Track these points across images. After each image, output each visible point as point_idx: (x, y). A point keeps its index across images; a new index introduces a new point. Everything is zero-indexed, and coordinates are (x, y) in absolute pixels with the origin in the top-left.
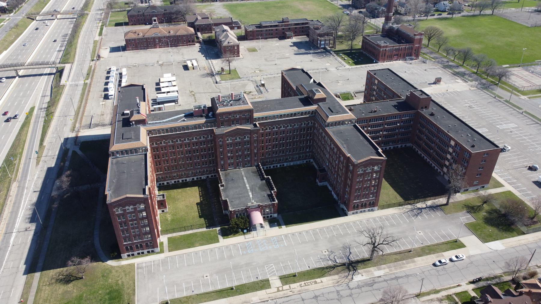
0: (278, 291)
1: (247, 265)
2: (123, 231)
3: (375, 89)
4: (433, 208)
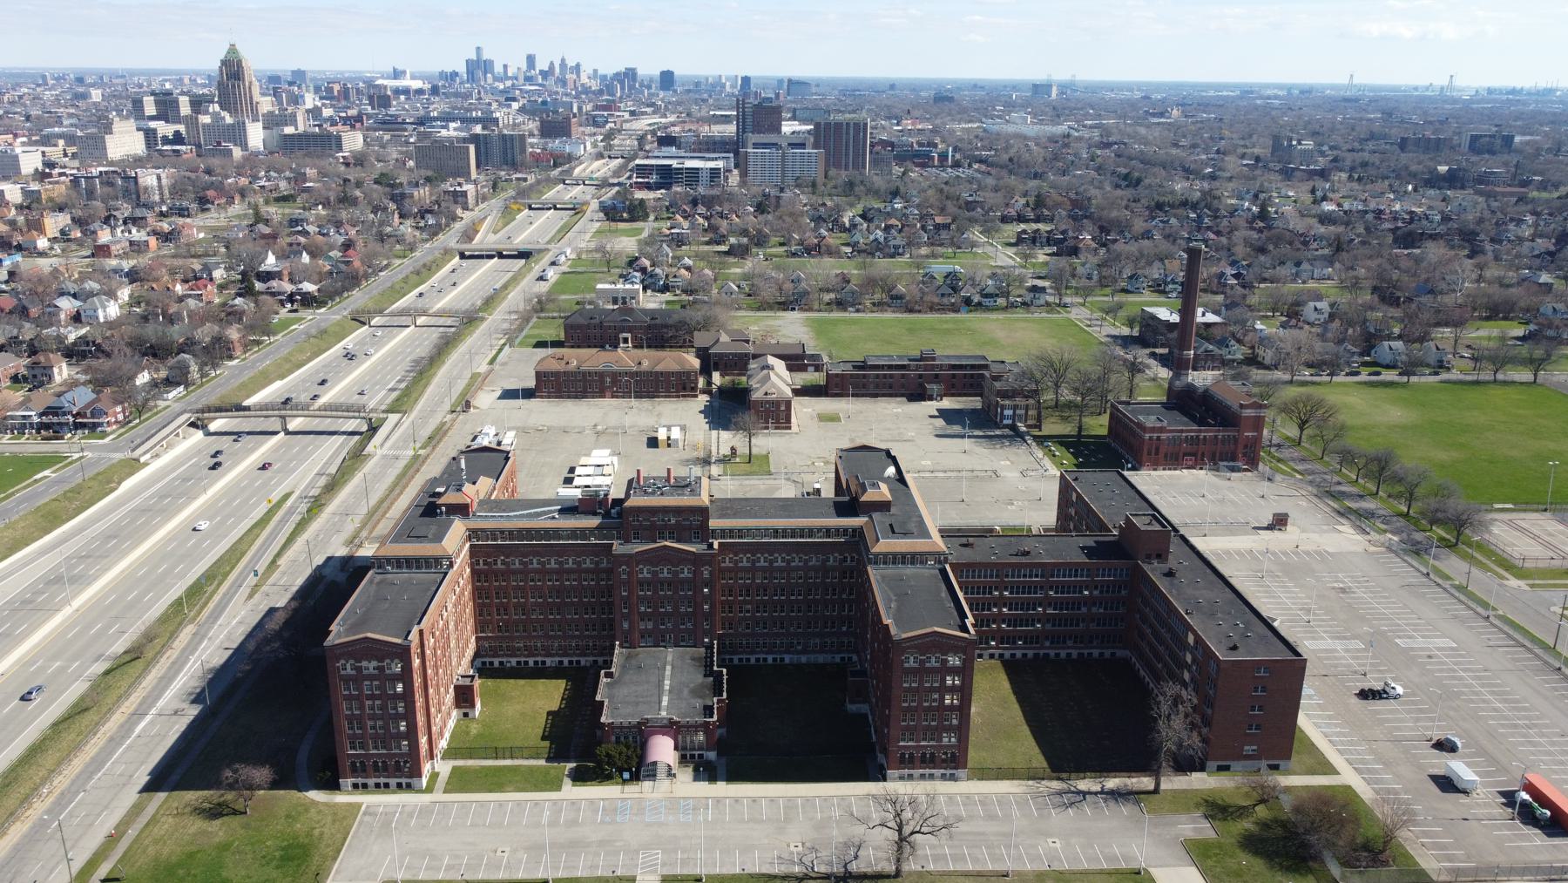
1: (601, 843)
2: (350, 719)
4: (1116, 795)
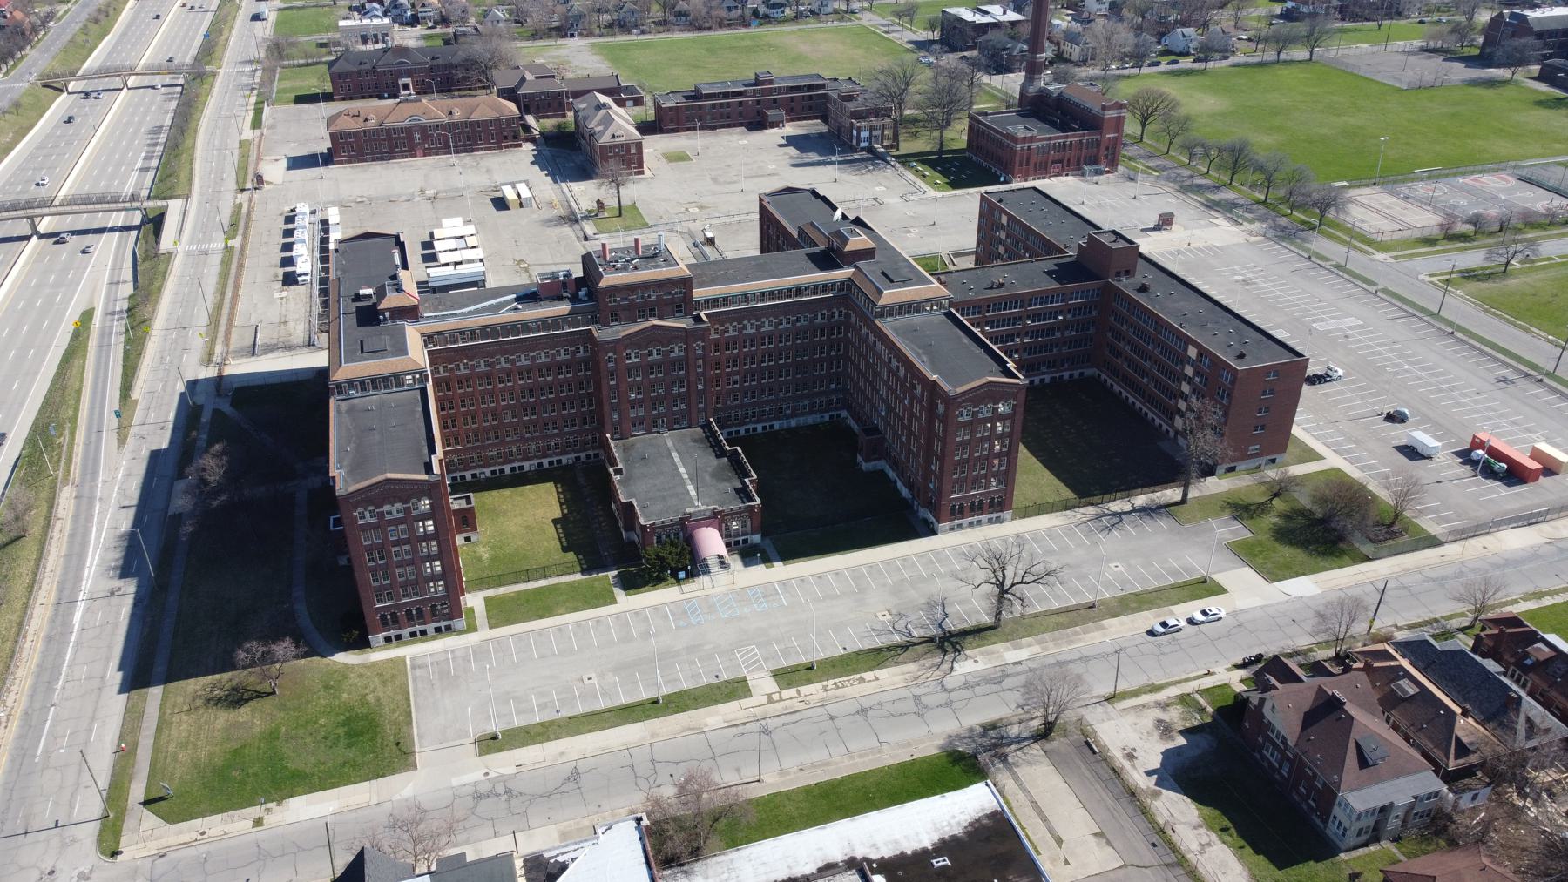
0: (771, 701)
1: (691, 649)
3: (999, 237)
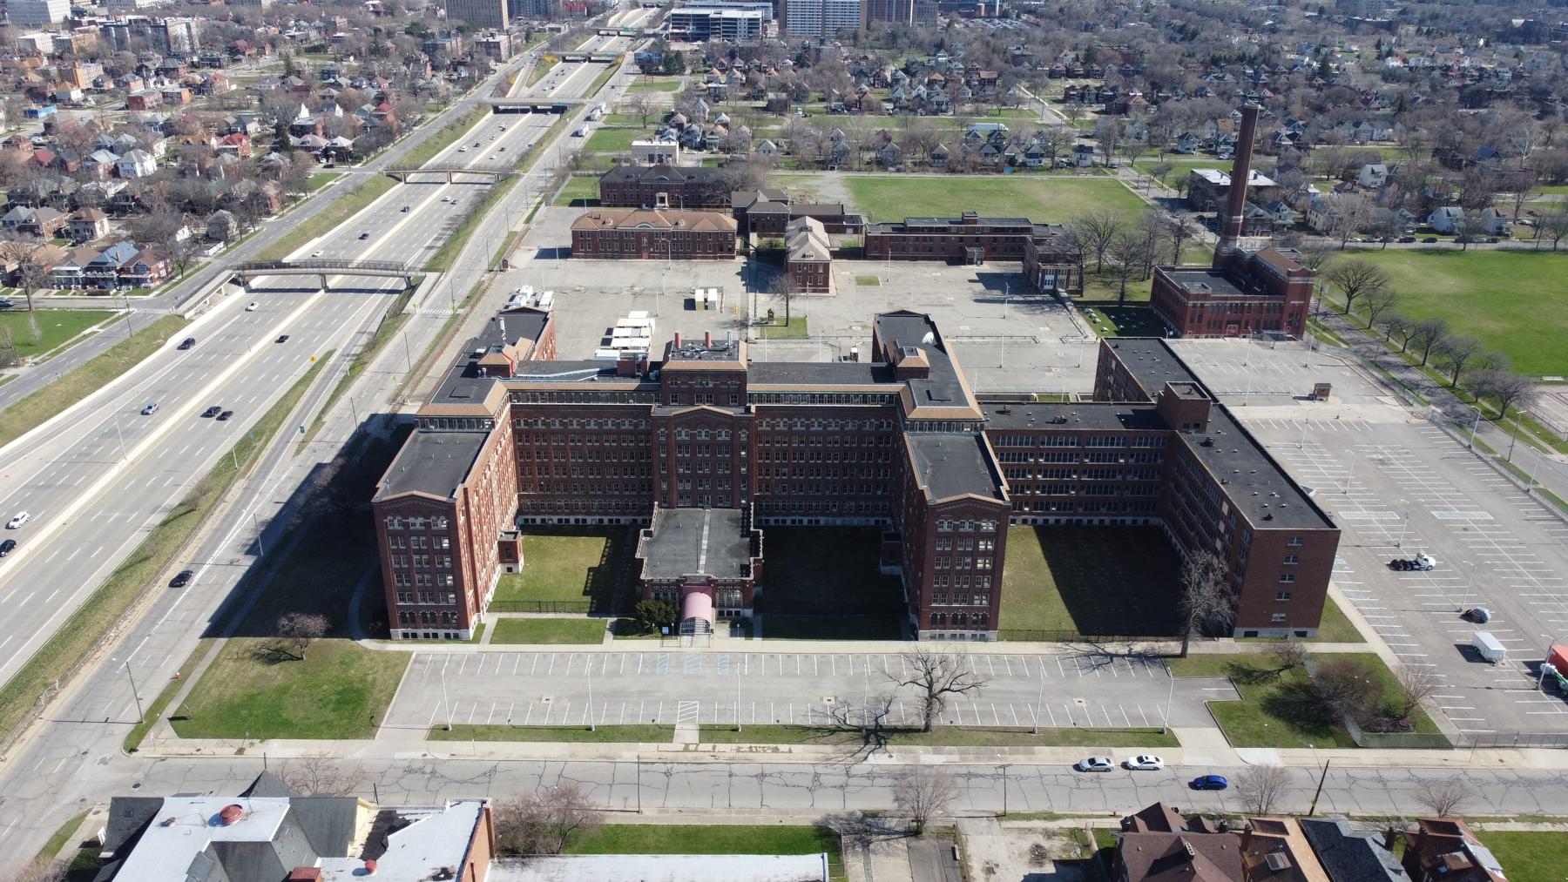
0: (686, 749)
1: (643, 693)
4: (1142, 658)
